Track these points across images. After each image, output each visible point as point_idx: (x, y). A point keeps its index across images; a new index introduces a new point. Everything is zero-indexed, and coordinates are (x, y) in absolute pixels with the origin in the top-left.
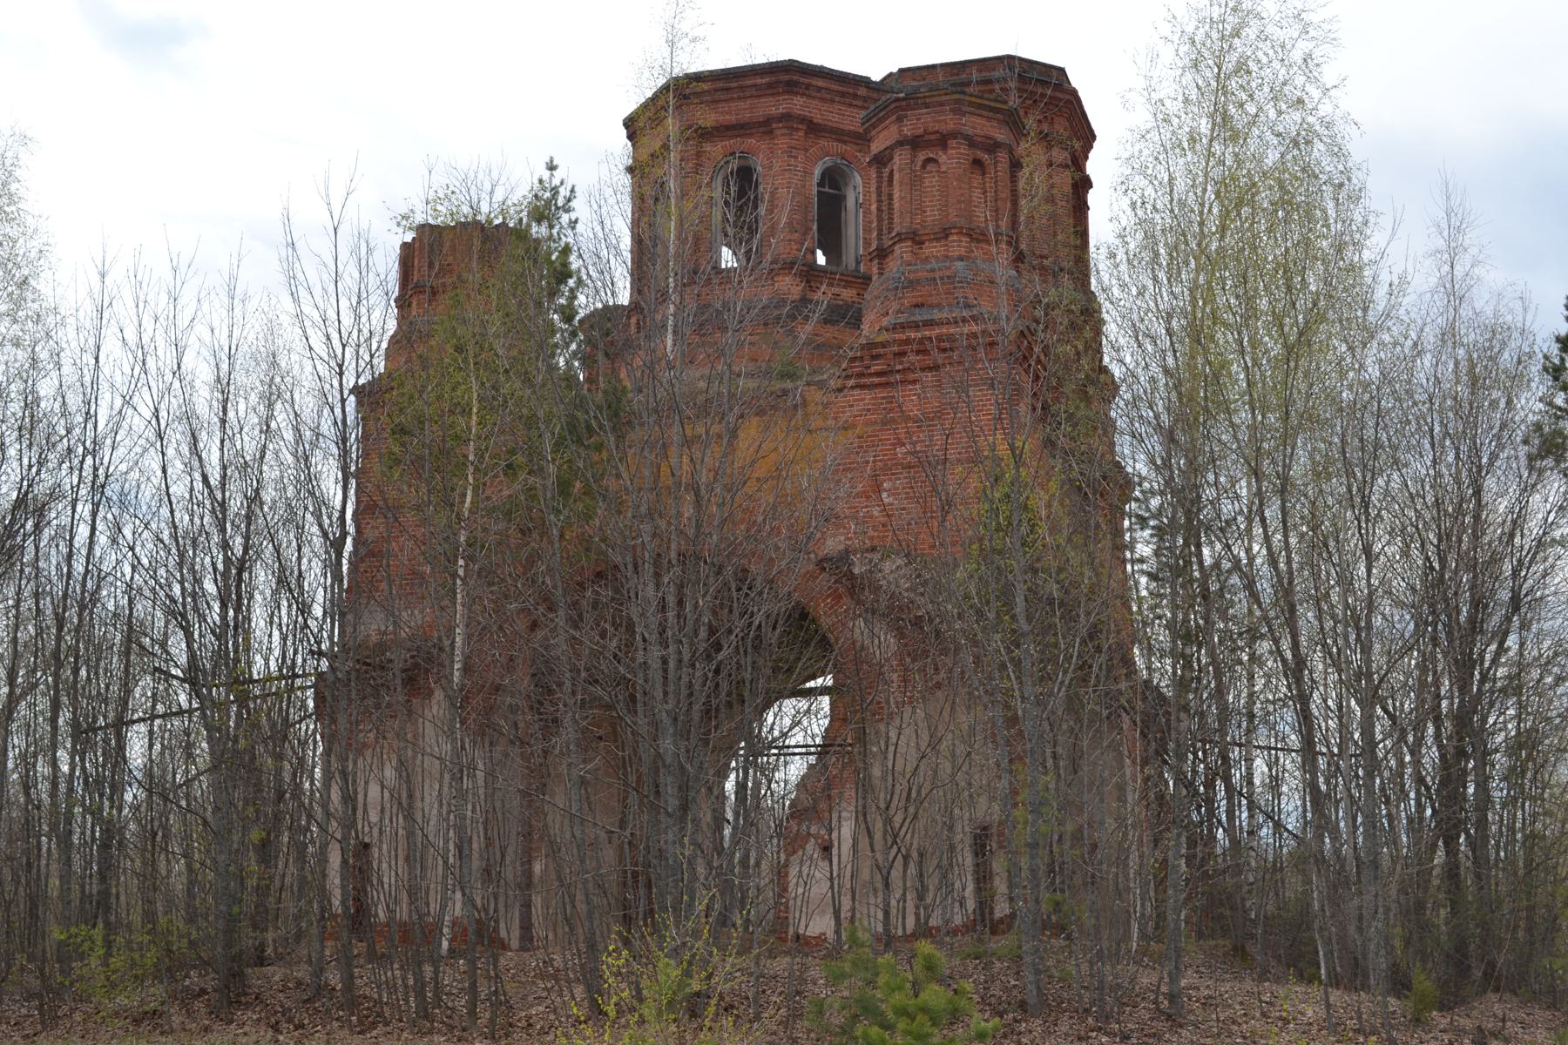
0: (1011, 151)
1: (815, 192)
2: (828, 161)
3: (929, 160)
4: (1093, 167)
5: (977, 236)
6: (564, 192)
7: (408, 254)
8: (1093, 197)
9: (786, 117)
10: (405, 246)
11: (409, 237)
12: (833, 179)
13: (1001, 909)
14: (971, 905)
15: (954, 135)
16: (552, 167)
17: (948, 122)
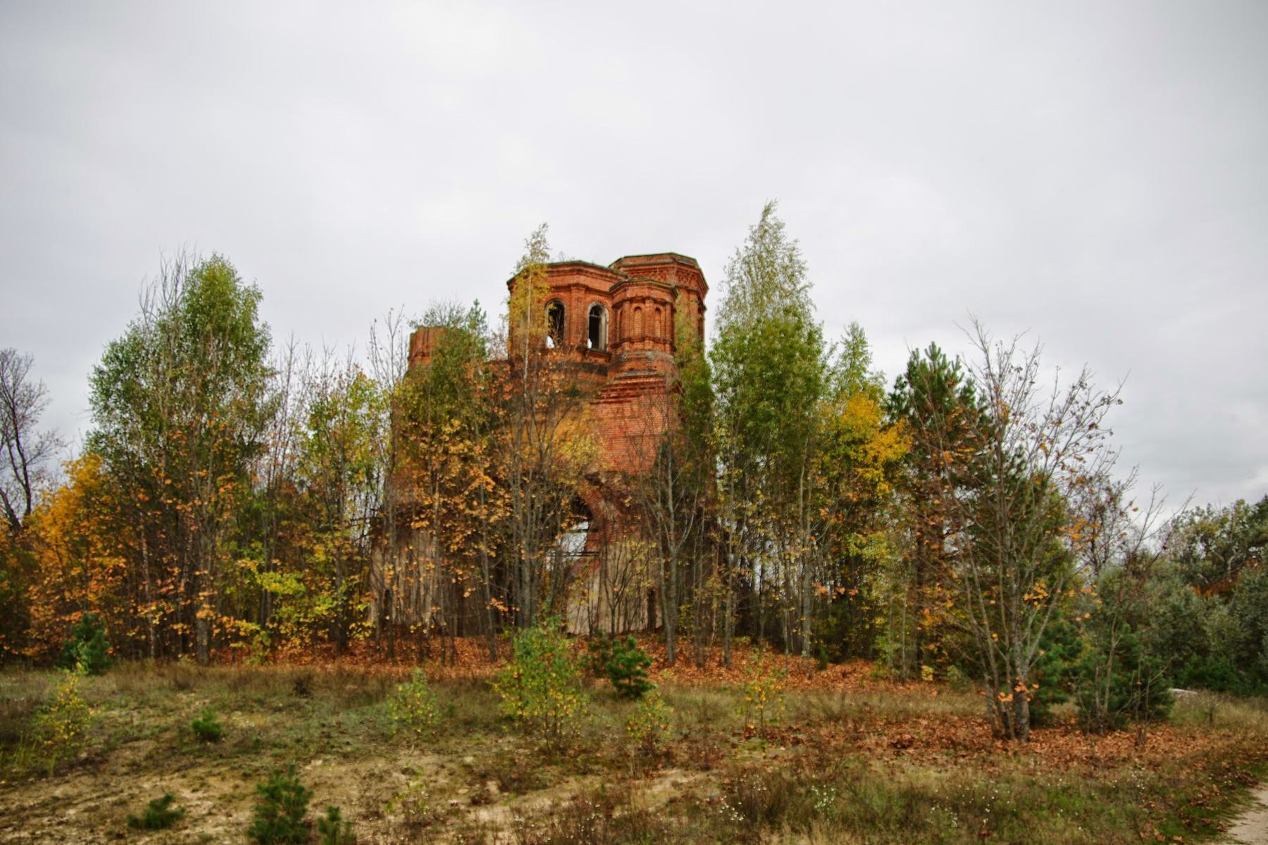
0: (672, 305)
1: (588, 316)
2: (594, 304)
3: (637, 308)
4: (706, 302)
5: (656, 341)
6: (482, 314)
7: (414, 338)
8: (706, 314)
9: (577, 285)
10: (412, 335)
11: (414, 331)
12: (597, 310)
13: (658, 624)
14: (646, 621)
15: (648, 298)
16: (476, 304)
17: (645, 292)
